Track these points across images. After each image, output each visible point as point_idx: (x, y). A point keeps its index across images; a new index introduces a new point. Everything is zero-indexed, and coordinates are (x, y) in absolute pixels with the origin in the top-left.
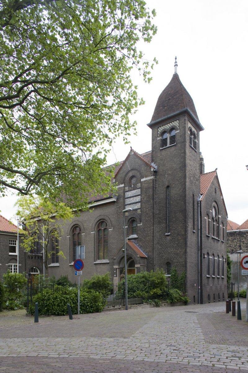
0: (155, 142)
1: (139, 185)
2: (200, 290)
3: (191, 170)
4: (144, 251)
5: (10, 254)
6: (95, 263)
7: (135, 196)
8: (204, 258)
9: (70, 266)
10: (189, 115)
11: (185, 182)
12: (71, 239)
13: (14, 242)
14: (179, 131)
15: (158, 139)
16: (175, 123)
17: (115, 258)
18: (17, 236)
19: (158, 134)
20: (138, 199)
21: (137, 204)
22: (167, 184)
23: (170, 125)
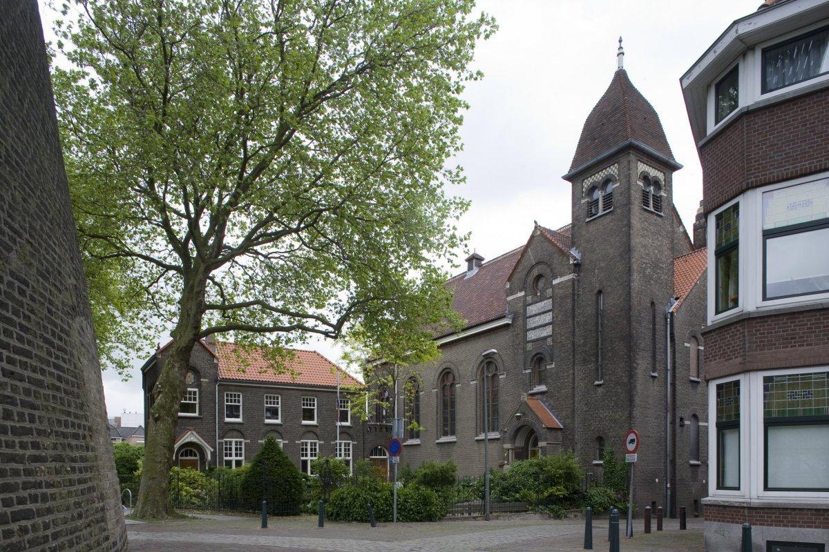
0: (577, 207)
1: (549, 291)
2: (669, 491)
3: (648, 254)
4: (557, 417)
5: (305, 422)
6: (476, 438)
7: (544, 313)
8: (682, 426)
9: (438, 444)
10: (640, 151)
11: (629, 281)
12: (439, 395)
13: (310, 401)
14: (618, 185)
15: (583, 201)
16: (612, 170)
17: (506, 430)
18: (336, 392)
19: (583, 192)
20: (548, 318)
22: (597, 287)
23: (604, 173)
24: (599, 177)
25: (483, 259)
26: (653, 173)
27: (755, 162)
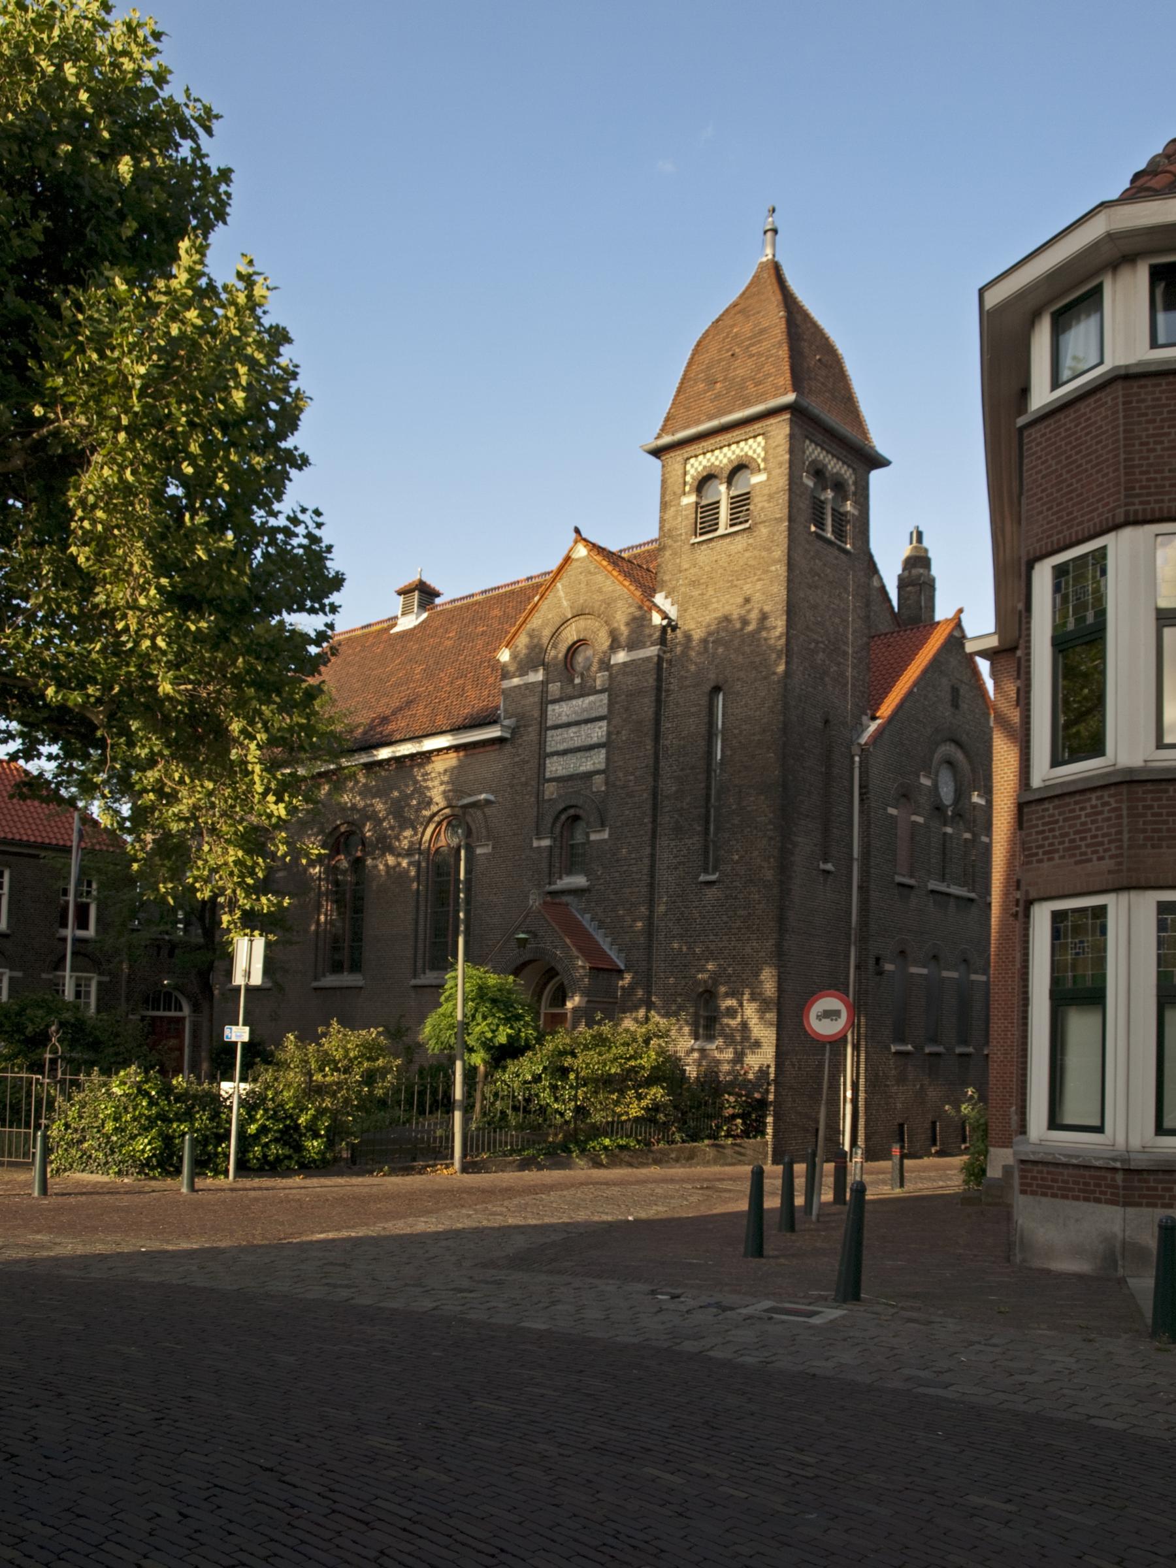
7: (587, 721)
8: (880, 973)
16: (751, 447)
19: (685, 483)
20: (598, 732)
21: (592, 752)
24: (722, 457)
25: (438, 595)
26: (834, 466)
27: (1142, 473)
